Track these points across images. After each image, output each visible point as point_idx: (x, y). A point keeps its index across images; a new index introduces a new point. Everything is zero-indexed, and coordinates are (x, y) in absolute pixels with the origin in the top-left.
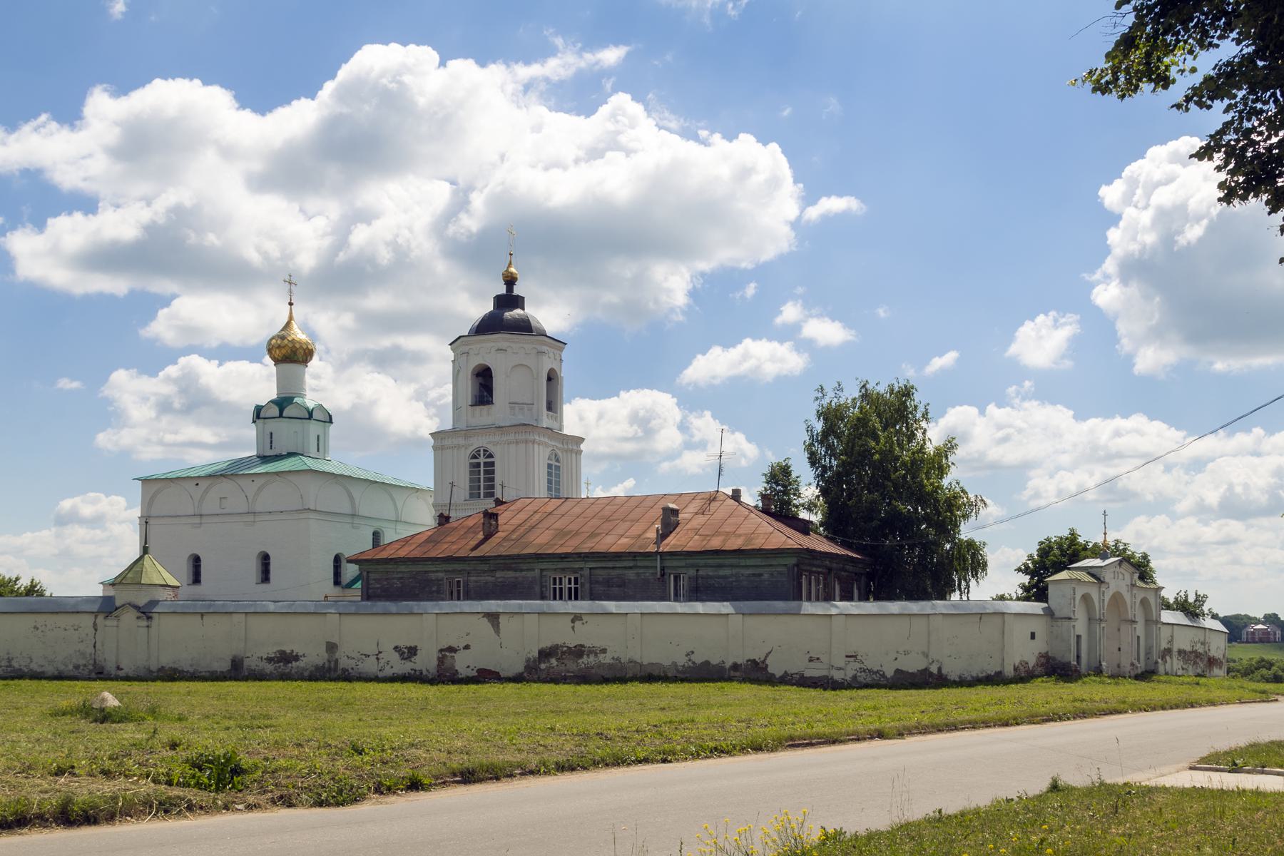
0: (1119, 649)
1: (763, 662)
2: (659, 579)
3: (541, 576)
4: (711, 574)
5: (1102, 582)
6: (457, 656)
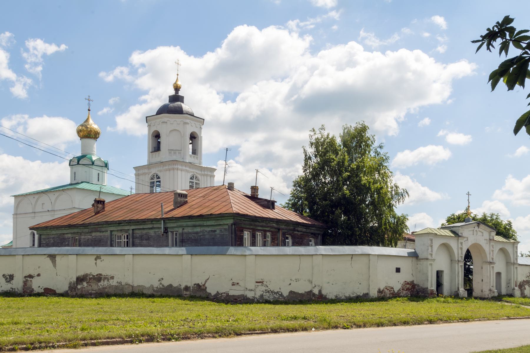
0: (482, 281)
1: (204, 285)
2: (163, 235)
3: (111, 235)
4: (190, 231)
5: (459, 236)
6: (34, 280)
